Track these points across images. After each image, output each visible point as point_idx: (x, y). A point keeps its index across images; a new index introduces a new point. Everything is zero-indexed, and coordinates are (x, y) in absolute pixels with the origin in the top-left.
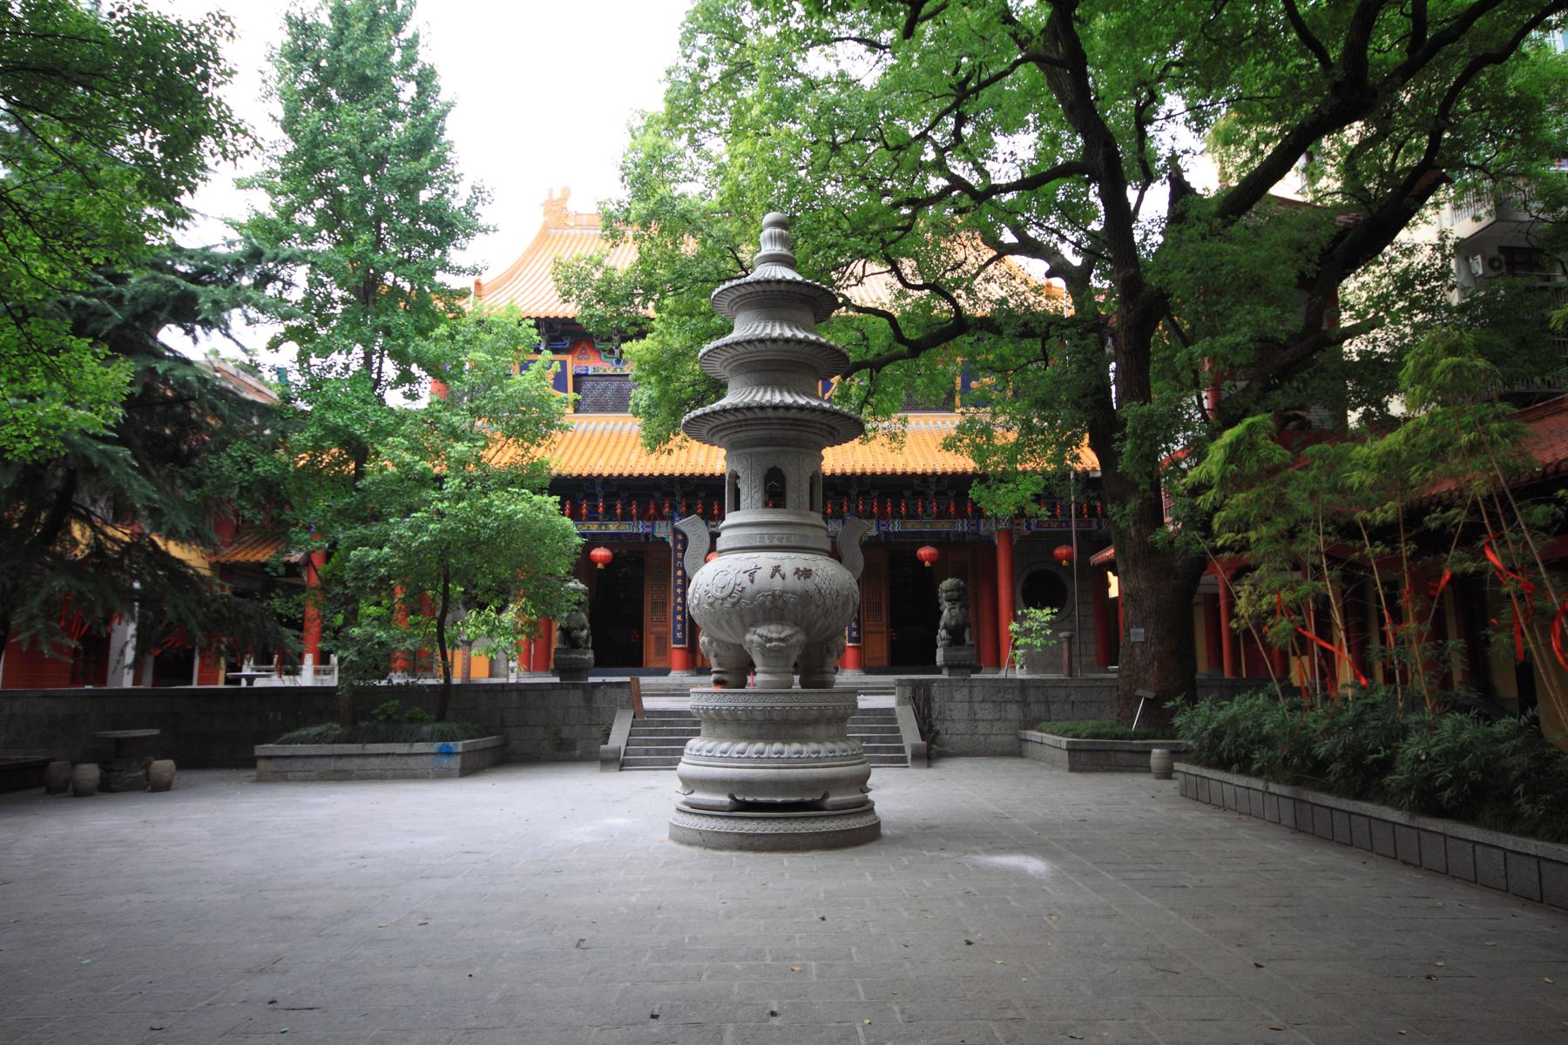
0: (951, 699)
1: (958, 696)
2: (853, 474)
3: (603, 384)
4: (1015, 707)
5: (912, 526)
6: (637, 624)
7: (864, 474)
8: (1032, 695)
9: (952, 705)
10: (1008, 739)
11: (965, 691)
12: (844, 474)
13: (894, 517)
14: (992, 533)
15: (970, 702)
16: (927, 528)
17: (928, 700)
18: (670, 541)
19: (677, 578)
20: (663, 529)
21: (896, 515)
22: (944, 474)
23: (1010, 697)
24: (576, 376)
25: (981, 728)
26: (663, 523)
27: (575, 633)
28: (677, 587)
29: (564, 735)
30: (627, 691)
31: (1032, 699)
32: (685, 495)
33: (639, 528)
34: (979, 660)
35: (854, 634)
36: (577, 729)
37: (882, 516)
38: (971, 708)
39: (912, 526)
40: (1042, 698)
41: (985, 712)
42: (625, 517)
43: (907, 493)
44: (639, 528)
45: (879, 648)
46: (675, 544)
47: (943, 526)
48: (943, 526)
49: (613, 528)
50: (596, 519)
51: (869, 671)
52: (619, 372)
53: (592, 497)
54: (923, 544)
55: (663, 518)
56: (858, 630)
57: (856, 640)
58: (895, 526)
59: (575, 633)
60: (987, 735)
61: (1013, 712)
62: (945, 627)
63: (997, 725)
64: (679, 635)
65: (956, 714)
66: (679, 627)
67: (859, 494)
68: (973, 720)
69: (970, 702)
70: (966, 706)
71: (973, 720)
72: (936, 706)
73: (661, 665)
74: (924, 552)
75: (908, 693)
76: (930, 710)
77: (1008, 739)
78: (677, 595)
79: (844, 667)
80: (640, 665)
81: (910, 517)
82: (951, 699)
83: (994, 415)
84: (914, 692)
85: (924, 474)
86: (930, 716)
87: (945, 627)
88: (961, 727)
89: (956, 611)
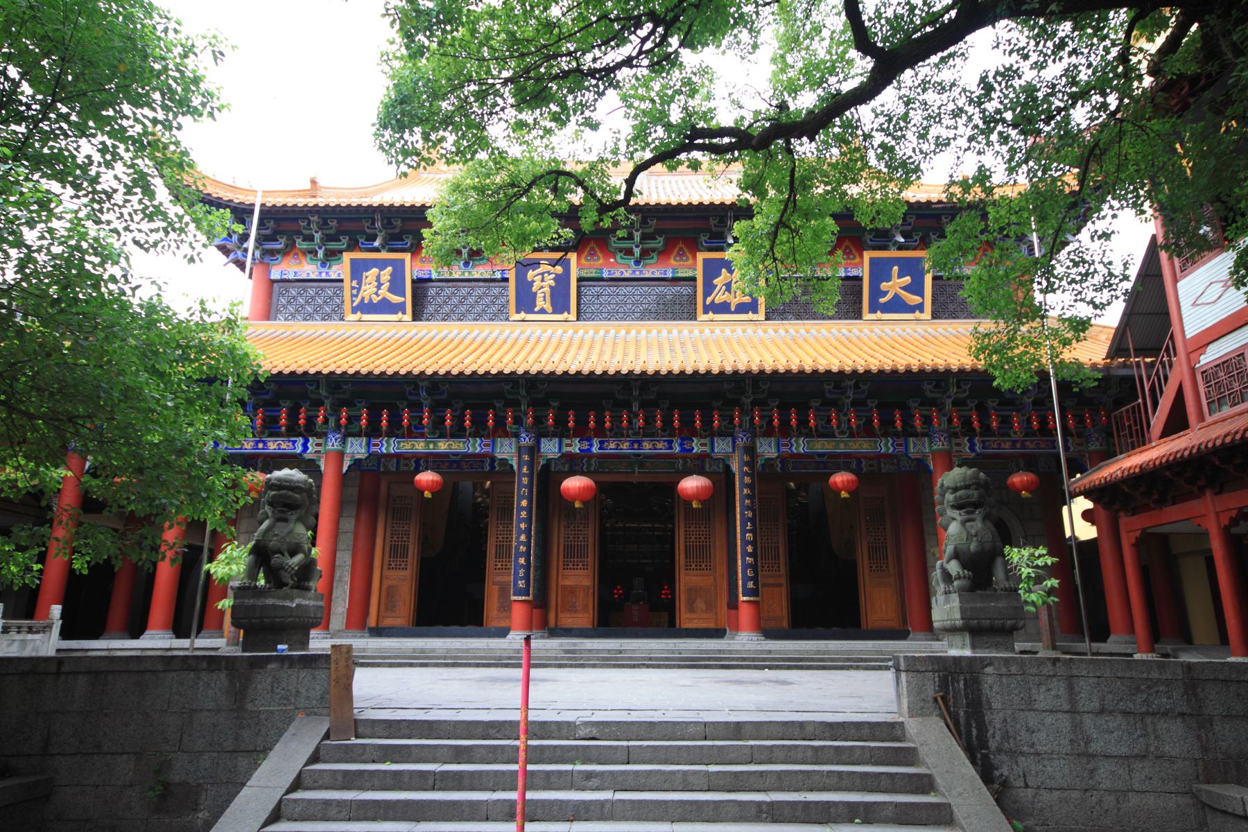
1: (1043, 699)
2: (749, 372)
3: (448, 291)
4: (1177, 727)
5: (822, 446)
7: (762, 372)
9: (1032, 719)
15: (1073, 711)
16: (841, 449)
18: (514, 463)
19: (520, 509)
20: (506, 449)
24: (417, 282)
26: (506, 441)
27: (276, 559)
28: (520, 521)
29: (176, 777)
30: (321, 675)
32: (533, 403)
33: (475, 446)
34: (905, 622)
35: (750, 585)
37: (785, 431)
38: (1076, 726)
39: (822, 446)
41: (1110, 736)
42: (458, 432)
43: (815, 403)
44: (475, 446)
45: (779, 605)
46: (520, 468)
47: (862, 446)
48: (862, 446)
49: (443, 446)
50: (422, 436)
51: (770, 634)
52: (467, 276)
54: (838, 469)
55: (506, 435)
57: (754, 592)
58: (800, 446)
62: (956, 555)
64: (521, 584)
65: (1043, 741)
66: (521, 572)
68: (1084, 754)
70: (1064, 722)
72: (995, 720)
73: (503, 624)
74: (840, 478)
75: (931, 690)
76: (982, 728)
78: (520, 532)
79: (737, 628)
80: (481, 625)
84: (944, 684)
85: (841, 373)
86: (983, 743)
87: (956, 555)
88: (1058, 771)
89: (978, 525)
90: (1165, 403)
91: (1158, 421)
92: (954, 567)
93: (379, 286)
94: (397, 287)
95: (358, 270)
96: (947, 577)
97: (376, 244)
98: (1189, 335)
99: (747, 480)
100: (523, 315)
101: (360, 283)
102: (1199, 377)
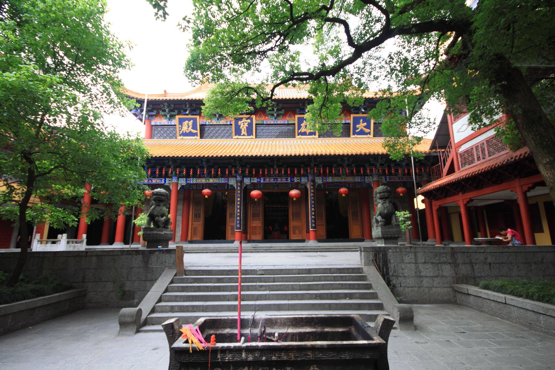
0: (402, 261)
1: (407, 259)
2: (313, 155)
4: (448, 267)
5: (336, 179)
6: (224, 223)
8: (460, 259)
9: (403, 266)
10: (445, 290)
11: (412, 256)
12: (308, 155)
13: (330, 176)
14: (371, 182)
15: (416, 263)
17: (386, 262)
18: (235, 186)
20: (232, 181)
21: (331, 174)
22: (352, 155)
23: (444, 259)
25: (425, 282)
26: (232, 179)
27: (157, 218)
28: (237, 205)
29: (127, 289)
30: (173, 256)
31: (460, 261)
33: (222, 181)
34: (363, 237)
35: (313, 225)
36: (136, 284)
37: (325, 175)
38: (417, 268)
39: (336, 179)
40: (467, 260)
41: (427, 270)
42: (216, 176)
43: (335, 165)
44: (222, 181)
45: (323, 232)
47: (350, 179)
48: (350, 179)
49: (211, 181)
51: (320, 241)
52: (218, 123)
53: (202, 168)
55: (232, 177)
56: (315, 223)
57: (315, 228)
59: (157, 218)
60: (430, 288)
61: (447, 270)
63: (437, 280)
64: (238, 226)
65: (406, 272)
66: (238, 222)
67: (315, 166)
68: (419, 276)
69: (416, 263)
70: (413, 266)
71: (419, 276)
72: (391, 266)
73: (232, 239)
74: (343, 190)
75: (371, 257)
76: (387, 269)
77: (445, 290)
79: (309, 239)
80: (349, 238)
81: (336, 176)
82: (402, 261)
83: (429, 61)
88: (410, 282)
90: (448, 164)
91: (445, 170)
92: (379, 218)
93: (188, 127)
94: (194, 127)
95: (181, 121)
96: (377, 221)
97: (187, 113)
98: (456, 141)
99: (312, 191)
100: (237, 137)
101: (182, 126)
102: (459, 156)
